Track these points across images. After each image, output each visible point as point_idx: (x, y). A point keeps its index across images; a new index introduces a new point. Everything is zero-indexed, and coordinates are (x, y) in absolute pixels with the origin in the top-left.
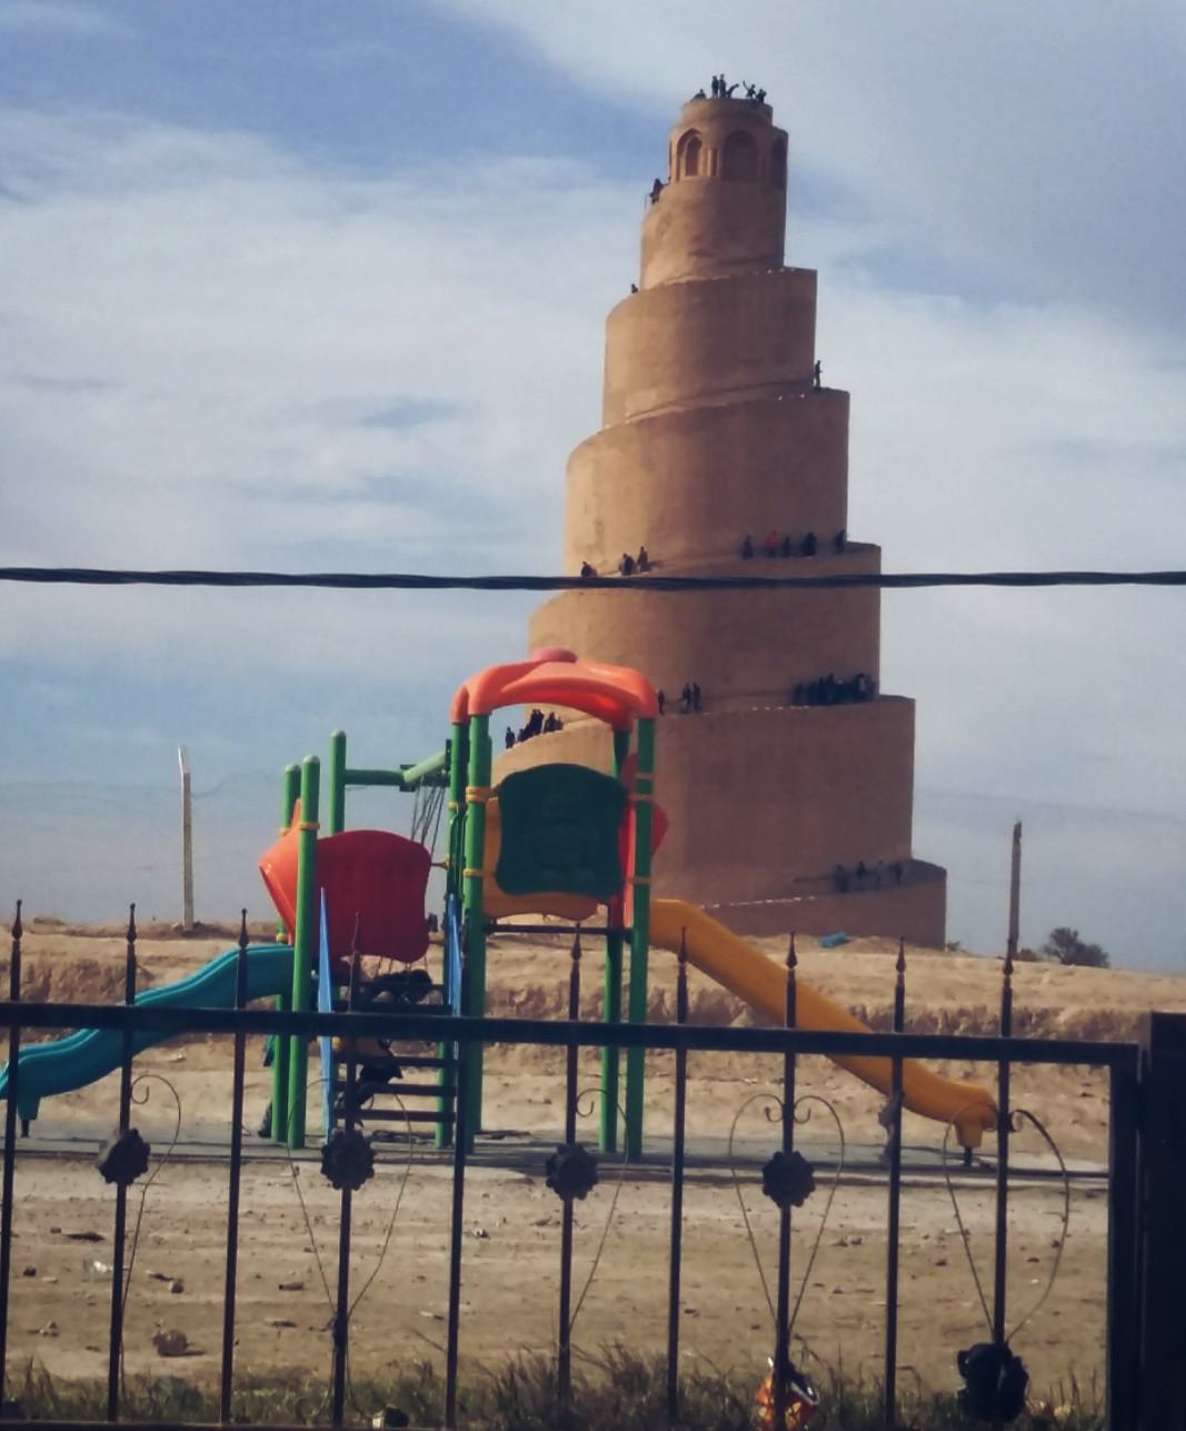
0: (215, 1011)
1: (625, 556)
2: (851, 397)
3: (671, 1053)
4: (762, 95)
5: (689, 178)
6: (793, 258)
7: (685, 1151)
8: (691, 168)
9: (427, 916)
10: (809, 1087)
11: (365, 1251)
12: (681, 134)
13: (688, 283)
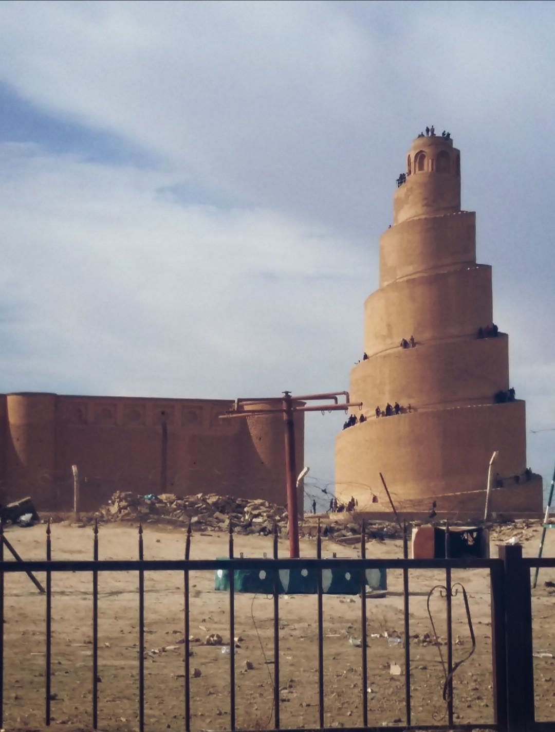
0: (445, 538)
1: (403, 339)
2: (509, 337)
4: (449, 135)
5: (420, 172)
6: (465, 206)
7: (409, 591)
8: (421, 168)
10: (211, 610)
11: (270, 650)
13: (426, 218)
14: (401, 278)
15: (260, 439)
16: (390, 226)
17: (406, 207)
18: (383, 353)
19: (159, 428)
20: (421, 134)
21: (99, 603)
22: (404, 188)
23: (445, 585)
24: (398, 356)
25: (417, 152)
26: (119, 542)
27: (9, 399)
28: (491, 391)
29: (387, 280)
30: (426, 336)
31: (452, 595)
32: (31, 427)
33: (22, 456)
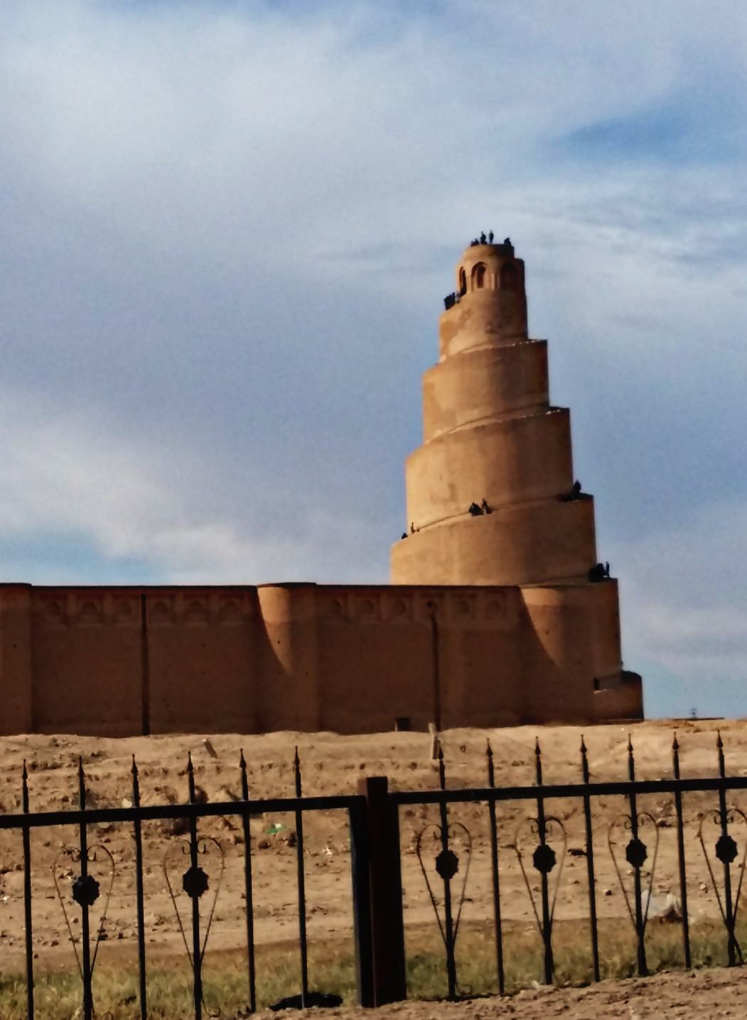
1: (473, 504)
3: (709, 798)
9: (574, 482)
12: (472, 266)
17: (461, 334)
19: (428, 624)
20: (478, 237)
22: (456, 312)
24: (467, 525)
27: (261, 592)
28: (583, 568)
30: (500, 499)
32: (293, 628)
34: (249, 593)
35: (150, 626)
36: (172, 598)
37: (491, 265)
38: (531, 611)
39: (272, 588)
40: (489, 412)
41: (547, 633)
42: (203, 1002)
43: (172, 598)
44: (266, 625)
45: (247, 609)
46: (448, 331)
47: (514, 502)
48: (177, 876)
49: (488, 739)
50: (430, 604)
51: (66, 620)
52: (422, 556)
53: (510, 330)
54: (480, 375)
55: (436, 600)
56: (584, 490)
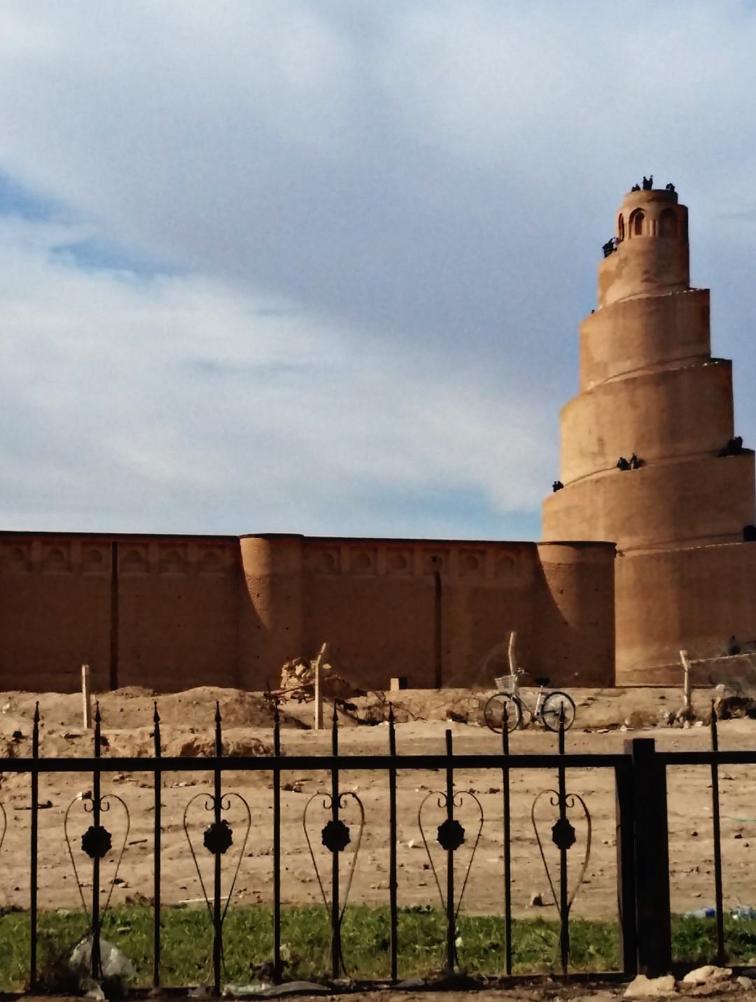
1: (621, 459)
5: (639, 236)
6: (696, 282)
13: (648, 299)
14: (615, 376)
15: (562, 592)
16: (593, 311)
18: (595, 477)
19: (431, 581)
21: (708, 810)
22: (614, 260)
23: (213, 794)
24: (614, 480)
25: (633, 210)
26: (422, 734)
27: (243, 541)
29: (594, 380)
31: (341, 807)
32: (273, 580)
33: (264, 617)
34: (232, 543)
35: (122, 575)
36: (146, 546)
37: (649, 209)
38: (545, 568)
39: (253, 539)
40: (642, 364)
41: (562, 592)
42: (457, 960)
43: (146, 546)
44: (247, 578)
45: (228, 559)
46: (607, 280)
47: (663, 457)
48: (546, 829)
49: (38, 703)
50: (434, 559)
51: (30, 566)
52: (568, 511)
53: (670, 279)
54: (634, 325)
55: (441, 556)
56: (745, 445)
